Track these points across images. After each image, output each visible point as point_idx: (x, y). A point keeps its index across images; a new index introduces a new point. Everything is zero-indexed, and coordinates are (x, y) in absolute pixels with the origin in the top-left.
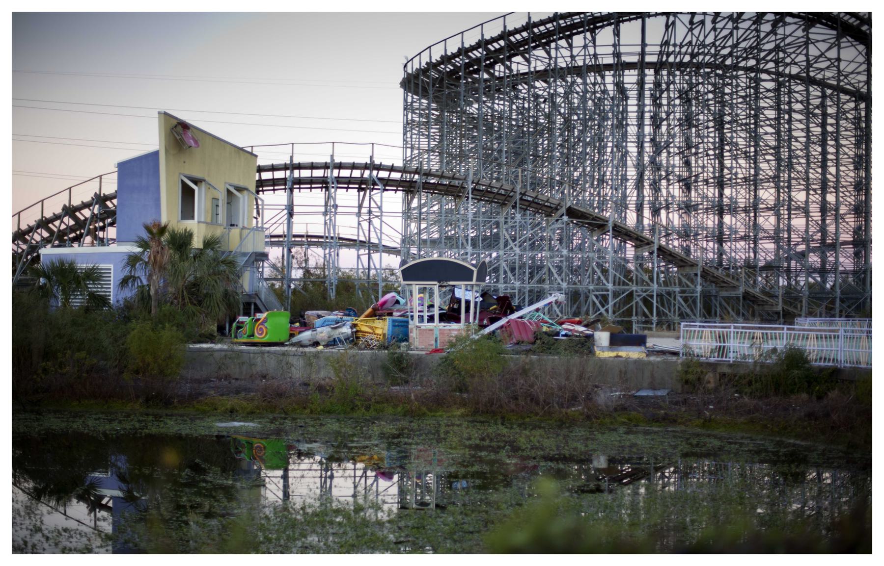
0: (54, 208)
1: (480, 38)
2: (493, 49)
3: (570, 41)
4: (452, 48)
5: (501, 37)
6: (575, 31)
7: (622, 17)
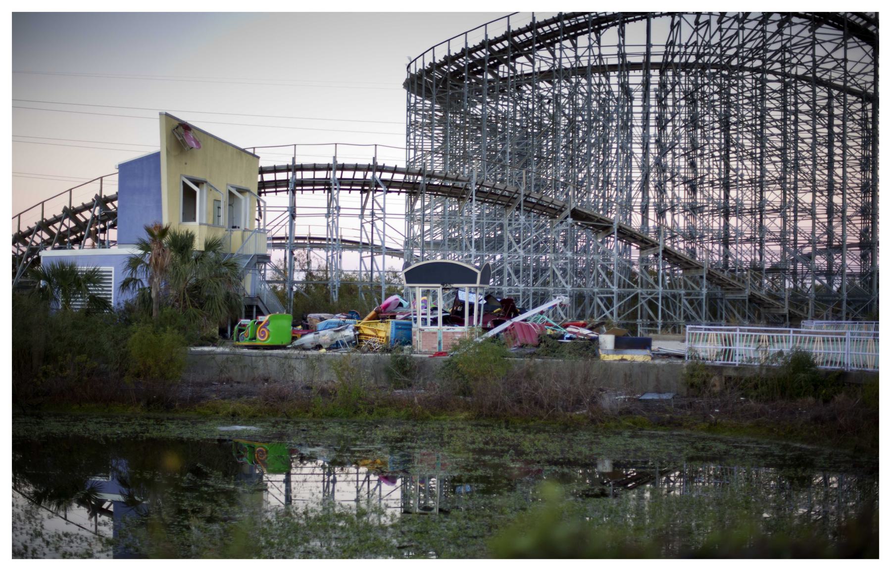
1: (484, 38)
2: (496, 49)
3: (575, 41)
4: (456, 49)
5: (505, 37)
6: (579, 31)
7: (627, 17)
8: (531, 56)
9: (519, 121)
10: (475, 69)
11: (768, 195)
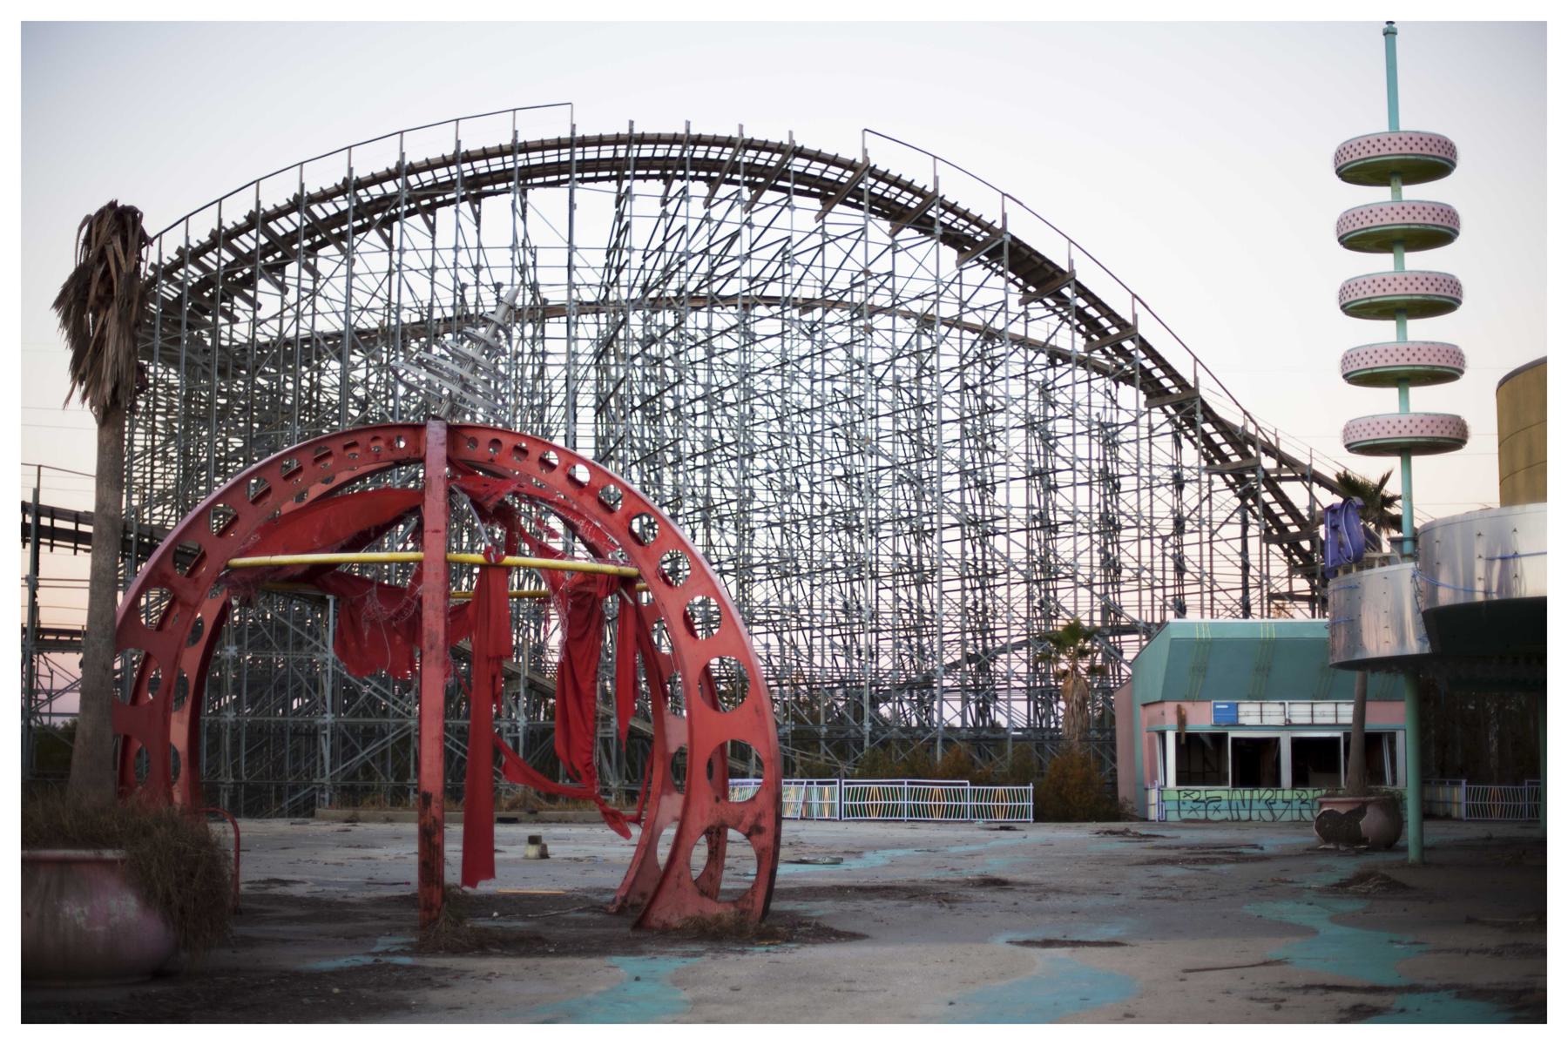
0: (276, 195)
1: (298, 191)
2: (321, 215)
3: (431, 218)
4: (235, 214)
5: (341, 190)
6: (439, 199)
7: (532, 177)
8: (250, 293)
9: (226, 465)
10: (239, 275)
11: (1064, 547)
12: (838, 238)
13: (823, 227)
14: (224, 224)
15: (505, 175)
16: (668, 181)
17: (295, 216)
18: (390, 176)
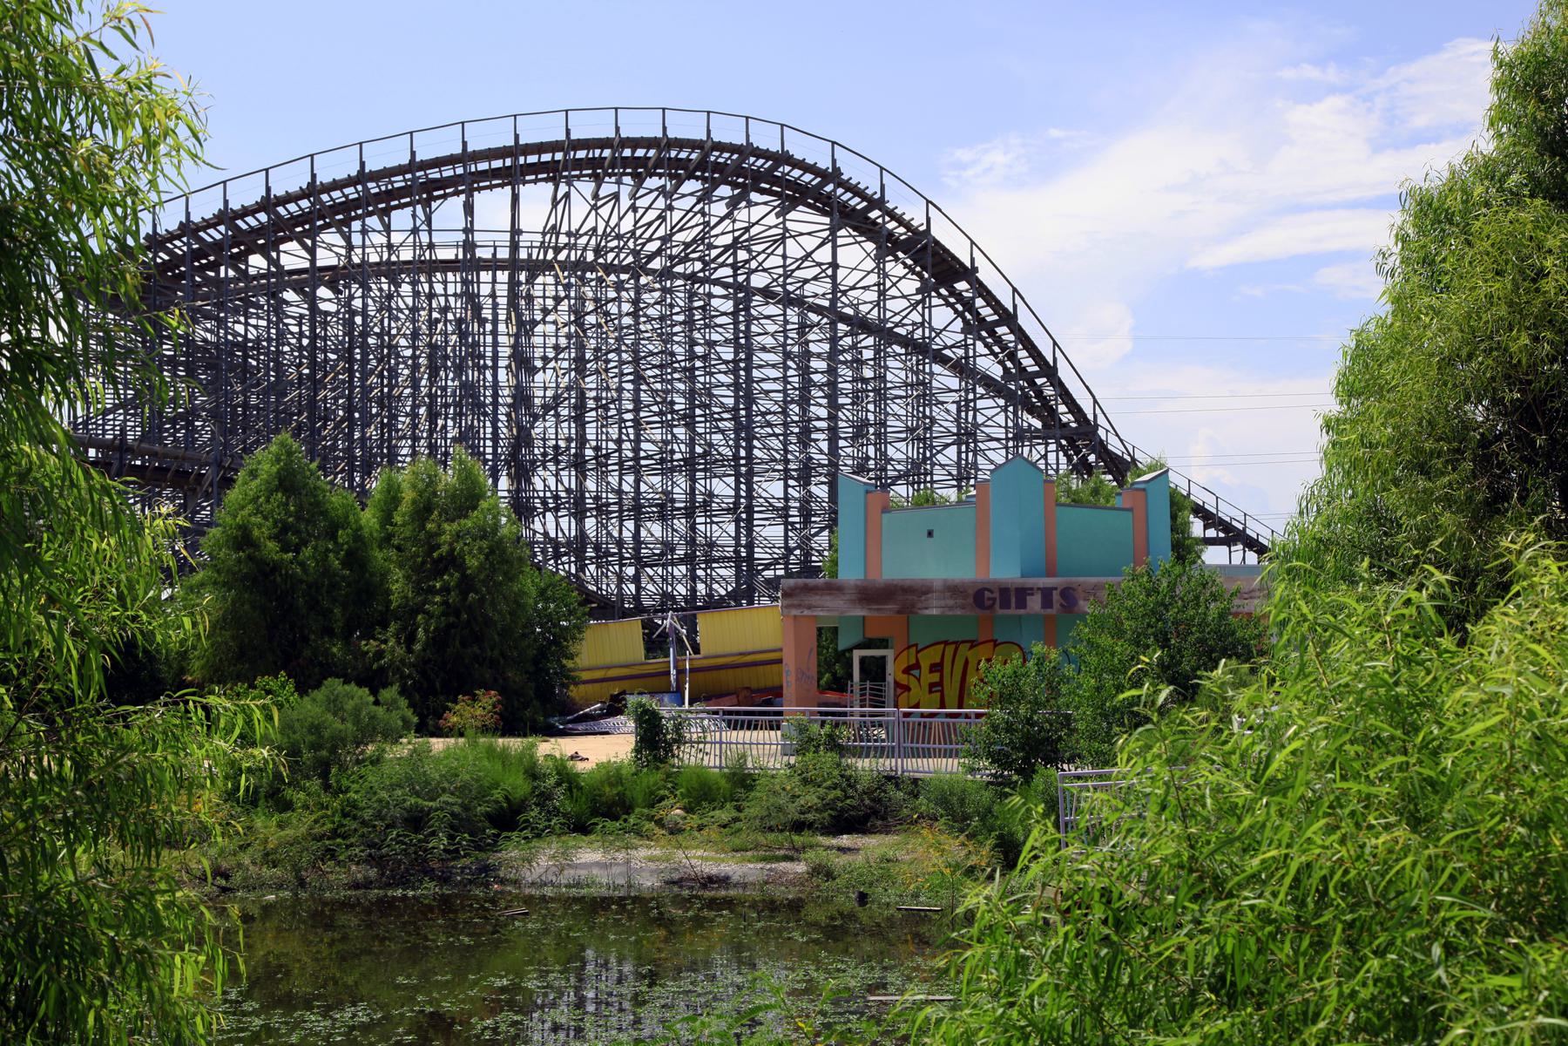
12: (801, 234)
13: (784, 223)
14: (159, 231)
15: (453, 181)
16: (599, 181)
17: (222, 228)
18: (350, 182)
